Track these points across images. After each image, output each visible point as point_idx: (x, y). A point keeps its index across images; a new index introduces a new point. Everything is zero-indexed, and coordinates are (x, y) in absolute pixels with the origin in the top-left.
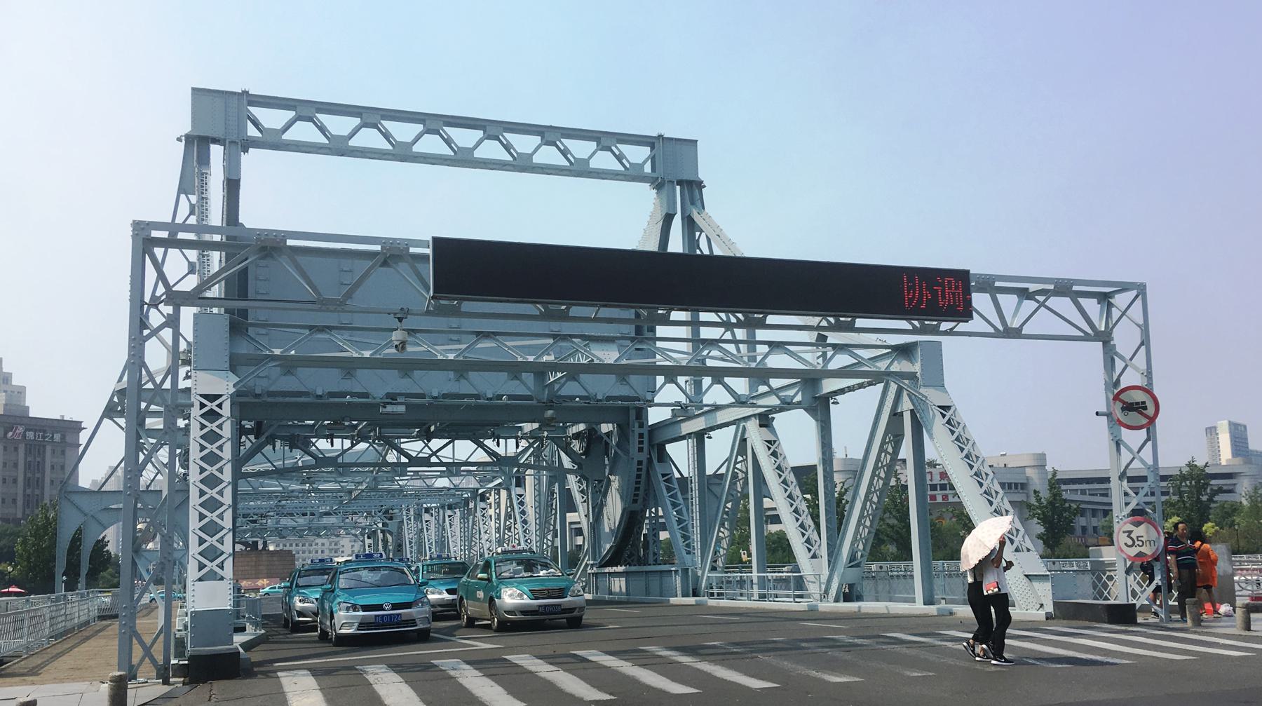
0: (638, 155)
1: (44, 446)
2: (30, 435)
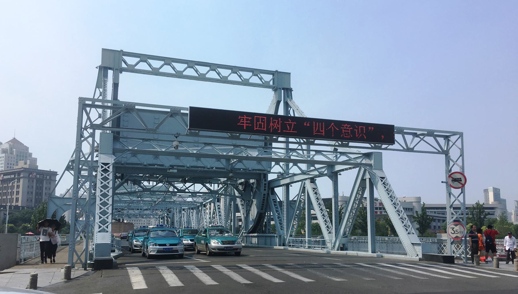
0: (268, 78)
1: (43, 181)
2: (38, 176)
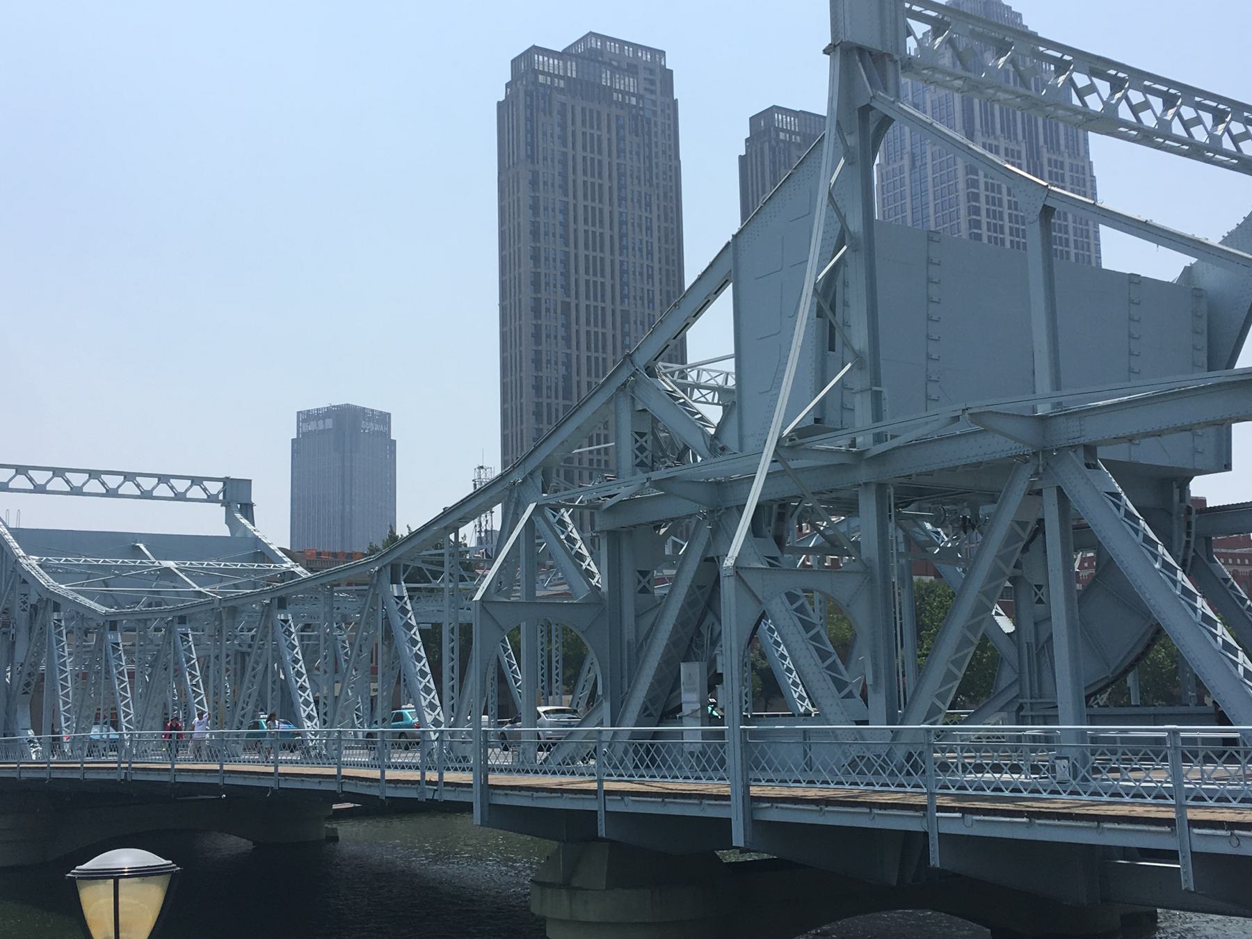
0: (215, 488)
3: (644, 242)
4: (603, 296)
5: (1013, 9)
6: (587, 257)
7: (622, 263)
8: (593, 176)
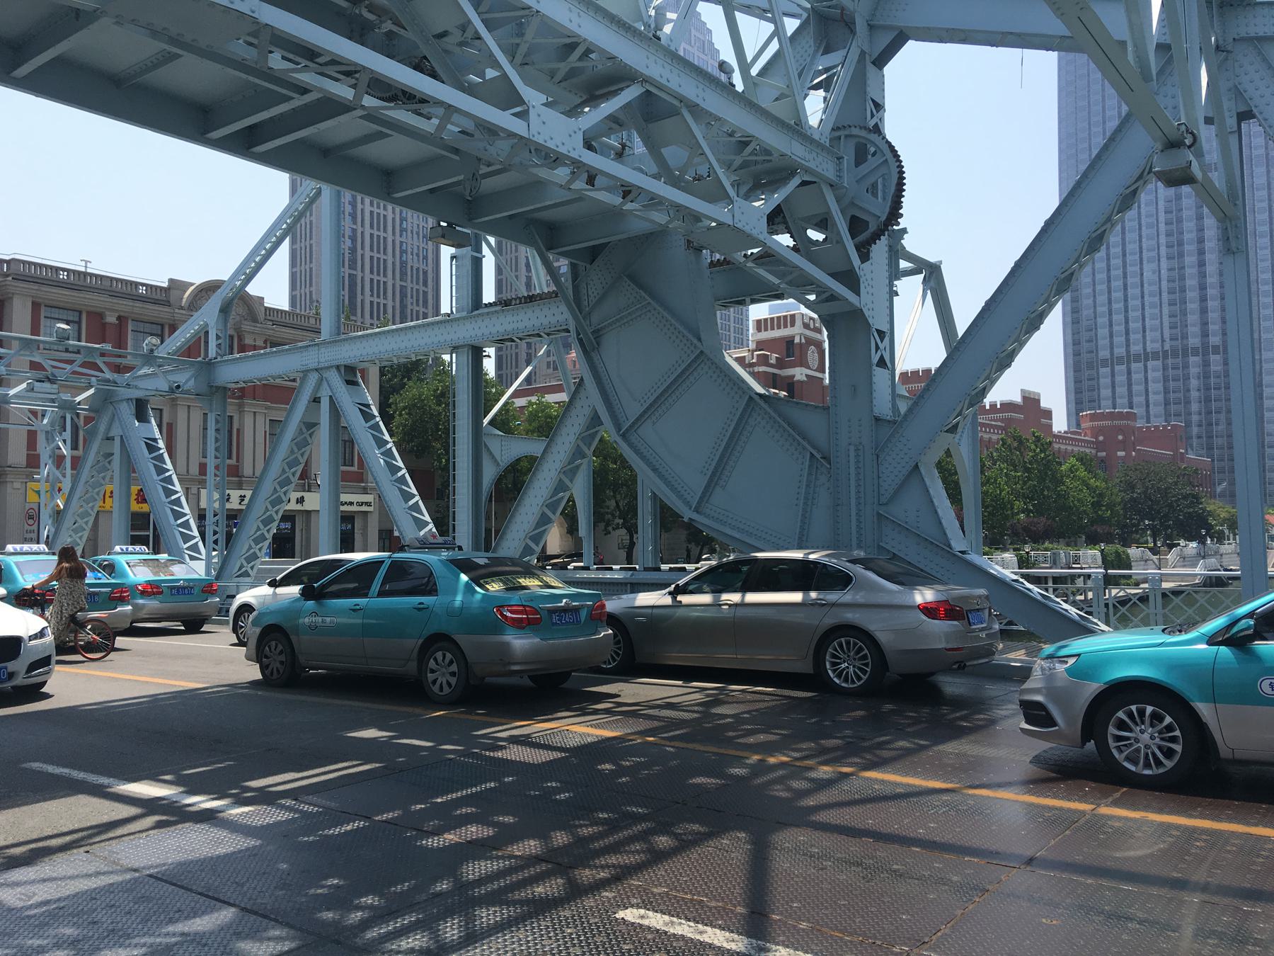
3: (421, 227)
4: (385, 249)
5: (708, 26)
6: (372, 280)
7: (401, 243)
8: (379, 252)
